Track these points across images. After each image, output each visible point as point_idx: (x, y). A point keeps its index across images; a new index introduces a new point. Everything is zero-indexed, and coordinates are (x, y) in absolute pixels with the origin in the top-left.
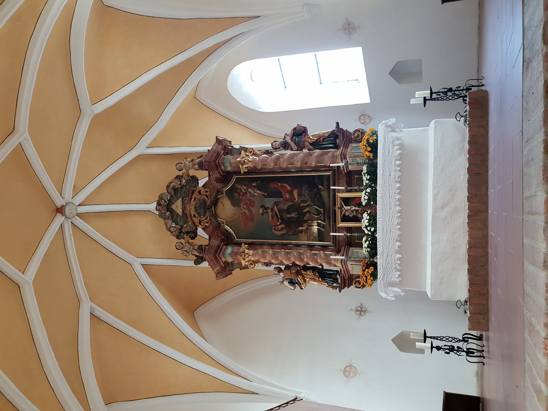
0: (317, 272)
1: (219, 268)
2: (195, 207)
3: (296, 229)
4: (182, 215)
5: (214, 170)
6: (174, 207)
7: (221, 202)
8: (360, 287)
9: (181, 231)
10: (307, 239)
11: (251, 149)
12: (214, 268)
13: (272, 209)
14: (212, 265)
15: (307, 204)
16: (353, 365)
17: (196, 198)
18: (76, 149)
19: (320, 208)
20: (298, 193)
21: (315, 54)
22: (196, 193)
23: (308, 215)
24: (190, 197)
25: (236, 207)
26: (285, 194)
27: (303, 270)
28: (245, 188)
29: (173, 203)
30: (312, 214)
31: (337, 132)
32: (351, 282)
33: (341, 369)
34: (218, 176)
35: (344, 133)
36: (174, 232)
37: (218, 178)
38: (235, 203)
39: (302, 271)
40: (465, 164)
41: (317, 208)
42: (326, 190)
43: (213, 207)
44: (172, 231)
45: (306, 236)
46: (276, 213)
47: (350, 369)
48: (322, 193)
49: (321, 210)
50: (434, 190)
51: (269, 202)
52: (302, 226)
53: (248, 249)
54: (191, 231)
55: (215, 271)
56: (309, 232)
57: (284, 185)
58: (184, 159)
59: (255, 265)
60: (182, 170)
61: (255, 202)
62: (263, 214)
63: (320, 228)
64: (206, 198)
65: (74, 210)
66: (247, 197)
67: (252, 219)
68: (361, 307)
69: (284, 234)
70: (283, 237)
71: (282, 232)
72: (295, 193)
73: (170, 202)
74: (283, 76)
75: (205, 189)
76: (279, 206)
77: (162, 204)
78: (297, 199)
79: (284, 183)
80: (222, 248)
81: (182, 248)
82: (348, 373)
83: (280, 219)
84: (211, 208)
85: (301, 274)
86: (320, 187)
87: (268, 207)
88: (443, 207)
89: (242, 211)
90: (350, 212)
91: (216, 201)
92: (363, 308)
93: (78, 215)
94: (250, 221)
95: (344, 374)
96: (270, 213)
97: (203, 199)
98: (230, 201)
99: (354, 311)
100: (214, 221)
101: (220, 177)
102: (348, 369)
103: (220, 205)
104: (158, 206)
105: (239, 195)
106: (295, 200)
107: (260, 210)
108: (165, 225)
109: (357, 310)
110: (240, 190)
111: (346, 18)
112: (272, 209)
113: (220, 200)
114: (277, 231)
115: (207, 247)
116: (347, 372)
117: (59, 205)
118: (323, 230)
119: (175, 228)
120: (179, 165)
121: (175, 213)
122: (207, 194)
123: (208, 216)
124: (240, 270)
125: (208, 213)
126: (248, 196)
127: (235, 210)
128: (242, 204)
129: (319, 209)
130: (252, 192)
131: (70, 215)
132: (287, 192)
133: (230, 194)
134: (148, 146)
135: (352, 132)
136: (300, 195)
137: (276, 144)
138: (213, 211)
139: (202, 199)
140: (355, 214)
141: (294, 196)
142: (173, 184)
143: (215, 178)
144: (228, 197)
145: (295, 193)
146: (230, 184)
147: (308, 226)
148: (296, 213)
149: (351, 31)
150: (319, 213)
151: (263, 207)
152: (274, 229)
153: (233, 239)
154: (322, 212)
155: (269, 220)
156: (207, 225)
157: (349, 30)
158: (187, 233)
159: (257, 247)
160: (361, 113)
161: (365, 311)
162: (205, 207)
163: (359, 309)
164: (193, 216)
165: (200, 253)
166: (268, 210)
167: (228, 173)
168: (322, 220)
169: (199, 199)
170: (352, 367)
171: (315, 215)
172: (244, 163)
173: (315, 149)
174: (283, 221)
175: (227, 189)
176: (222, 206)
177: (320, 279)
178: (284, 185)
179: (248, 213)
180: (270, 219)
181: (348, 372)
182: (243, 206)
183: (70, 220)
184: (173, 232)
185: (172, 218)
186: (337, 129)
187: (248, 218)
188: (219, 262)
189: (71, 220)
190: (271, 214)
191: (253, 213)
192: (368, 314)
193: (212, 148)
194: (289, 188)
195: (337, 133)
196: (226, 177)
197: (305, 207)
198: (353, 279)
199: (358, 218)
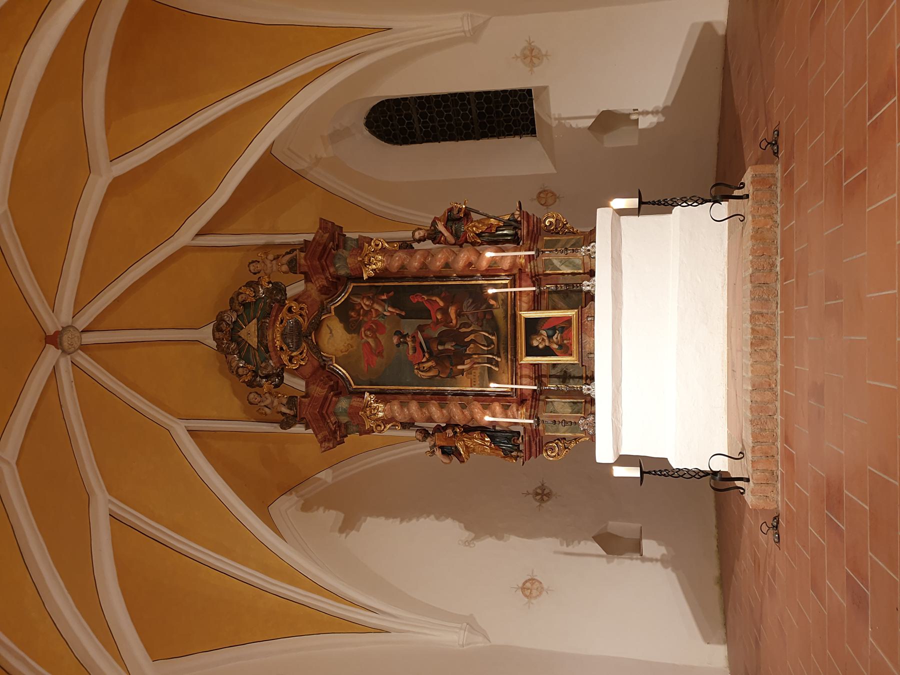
0: (487, 435)
1: (326, 433)
3: (454, 369)
6: (243, 334)
9: (255, 374)
10: (471, 383)
12: (318, 433)
13: (413, 337)
14: (315, 428)
16: (535, 578)
19: (493, 336)
20: (456, 311)
23: (472, 345)
25: (353, 335)
26: (436, 313)
27: (464, 432)
30: (478, 345)
33: (517, 585)
34: (325, 283)
37: (324, 286)
38: (351, 327)
41: (487, 335)
42: (501, 307)
44: (240, 373)
45: (469, 380)
46: (421, 343)
47: (532, 585)
48: (495, 311)
49: (493, 338)
51: (409, 326)
52: (463, 364)
54: (273, 373)
55: (320, 437)
56: (474, 373)
57: (434, 298)
60: (259, 272)
61: (386, 325)
62: (398, 345)
63: (492, 367)
64: (300, 319)
65: (76, 339)
67: (380, 354)
69: (432, 377)
71: (431, 374)
72: (452, 311)
73: (235, 327)
76: (425, 333)
77: (224, 329)
78: (454, 322)
79: (433, 295)
81: (259, 402)
82: (529, 591)
87: (408, 334)
90: (540, 341)
91: (318, 324)
92: (545, 489)
93: (84, 348)
94: (378, 356)
95: (523, 593)
98: (342, 325)
99: (531, 495)
101: (327, 285)
102: (528, 585)
103: (325, 331)
104: (217, 333)
105: (359, 315)
106: (452, 322)
107: (393, 339)
108: (228, 363)
109: (537, 494)
110: (360, 306)
111: (528, 40)
112: (414, 338)
114: (422, 372)
115: (306, 400)
117: (51, 330)
119: (245, 369)
121: (245, 344)
124: (360, 435)
125: (304, 344)
126: (374, 316)
128: (363, 329)
129: (489, 336)
130: (380, 309)
131: (70, 347)
132: (438, 309)
133: (343, 313)
136: (459, 315)
138: (314, 341)
140: (547, 344)
141: (451, 317)
143: (320, 286)
144: (338, 318)
145: (452, 311)
148: (454, 344)
150: (490, 342)
151: (398, 333)
152: (416, 369)
153: (348, 385)
154: (495, 342)
155: (409, 354)
156: (303, 363)
157: (531, 59)
159: (388, 397)
161: (549, 495)
162: (299, 334)
163: (539, 491)
166: (407, 339)
167: (338, 278)
168: (495, 354)
170: (534, 582)
171: (484, 346)
176: (329, 332)
178: (434, 298)
179: (373, 344)
180: (411, 352)
181: (529, 589)
182: (365, 331)
183: (69, 357)
184: (243, 375)
187: (374, 351)
188: (326, 423)
189: (71, 358)
190: (413, 345)
191: (382, 344)
193: (314, 239)
194: (442, 304)
195: (518, 218)
197: (468, 334)
198: (543, 445)
199: (553, 351)
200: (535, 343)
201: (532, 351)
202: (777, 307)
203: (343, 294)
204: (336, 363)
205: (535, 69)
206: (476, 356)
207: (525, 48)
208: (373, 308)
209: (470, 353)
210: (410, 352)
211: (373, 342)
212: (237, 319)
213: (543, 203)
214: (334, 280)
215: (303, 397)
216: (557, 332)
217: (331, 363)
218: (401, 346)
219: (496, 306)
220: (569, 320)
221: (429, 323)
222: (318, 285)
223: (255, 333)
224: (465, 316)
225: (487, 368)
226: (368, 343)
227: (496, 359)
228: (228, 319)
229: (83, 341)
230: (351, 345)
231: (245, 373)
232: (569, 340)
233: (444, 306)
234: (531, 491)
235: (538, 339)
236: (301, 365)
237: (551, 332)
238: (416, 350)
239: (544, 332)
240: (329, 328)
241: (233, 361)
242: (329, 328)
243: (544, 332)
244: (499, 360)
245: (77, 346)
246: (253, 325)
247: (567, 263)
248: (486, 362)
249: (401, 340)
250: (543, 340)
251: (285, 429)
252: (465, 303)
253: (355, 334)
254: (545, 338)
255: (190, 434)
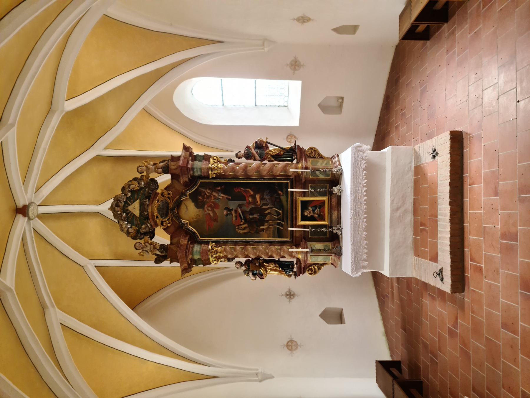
2: (158, 209)
4: (140, 216)
5: (185, 174)
7: (185, 204)
8: (313, 274)
11: (215, 157)
15: (268, 206)
16: (293, 339)
17: (160, 200)
18: (43, 145)
21: (255, 81)
22: (160, 195)
23: (269, 216)
24: (152, 199)
25: (200, 209)
26: (248, 198)
28: (209, 191)
29: (130, 205)
31: (294, 148)
32: (305, 270)
34: (187, 180)
35: (301, 150)
36: (132, 233)
37: (186, 182)
38: (199, 205)
39: (265, 263)
40: (412, 179)
41: (277, 210)
43: (176, 209)
45: (267, 234)
46: (240, 214)
47: (292, 344)
49: (280, 211)
50: (391, 197)
51: (233, 205)
52: (264, 225)
53: (216, 247)
54: (150, 232)
55: (182, 268)
56: (270, 230)
58: (145, 163)
59: (218, 261)
61: (220, 204)
62: (227, 215)
63: (280, 227)
66: (211, 199)
68: (290, 291)
70: (245, 235)
71: (245, 231)
72: (258, 197)
74: (222, 95)
75: (168, 191)
78: (259, 202)
79: (247, 188)
80: (190, 247)
82: (291, 347)
83: (244, 219)
84: (175, 210)
85: (264, 266)
86: (280, 192)
87: (232, 209)
88: (398, 209)
89: (206, 213)
90: (308, 213)
96: (234, 215)
97: (165, 201)
100: (177, 222)
102: (290, 344)
103: (183, 207)
105: (204, 198)
106: (257, 203)
108: (120, 226)
109: (287, 295)
110: (204, 193)
112: (236, 211)
113: (186, 202)
114: (240, 230)
116: (290, 346)
117: (21, 203)
118: (282, 228)
120: (140, 168)
122: (170, 196)
123: (170, 217)
125: (170, 214)
126: (213, 198)
127: (199, 212)
128: (206, 206)
129: (278, 211)
130: (216, 195)
133: (194, 198)
134: (105, 148)
135: (307, 149)
136: (262, 199)
137: (240, 154)
139: (164, 201)
140: (312, 214)
142: (133, 186)
145: (258, 197)
146: (194, 188)
147: (269, 225)
148: (258, 215)
149: (297, 67)
150: (278, 214)
151: (227, 209)
152: (237, 228)
155: (233, 220)
156: (169, 225)
158: (145, 234)
160: (289, 133)
161: (294, 295)
163: (288, 293)
164: (156, 217)
165: (161, 252)
168: (281, 220)
169: (162, 201)
172: (215, 170)
173: (275, 161)
174: (246, 221)
175: (191, 192)
176: (185, 207)
177: (281, 270)
178: (248, 190)
179: (212, 214)
180: (234, 219)
182: (207, 207)
184: (131, 232)
185: (128, 220)
186: (295, 146)
187: (212, 219)
190: (235, 215)
191: (218, 214)
192: (296, 297)
194: (252, 193)
196: (194, 180)
200: (306, 214)
201: (304, 218)
202: (360, 197)
203: (195, 186)
204: (189, 225)
205: (296, 72)
206: (271, 221)
207: (292, 61)
208: (212, 194)
209: (268, 219)
210: (233, 219)
211: (212, 213)
212: (126, 200)
213: (289, 141)
214: (191, 178)
215: (170, 245)
216: (318, 208)
217: (187, 225)
218: (228, 216)
219: (282, 194)
220: (323, 202)
221: (245, 203)
222: (183, 181)
223: (138, 208)
224: (265, 200)
225: (276, 227)
226: (209, 214)
227: (282, 223)
228: (121, 200)
229: (39, 211)
230: (199, 215)
231: (132, 231)
232: (324, 212)
233: (254, 194)
234: (284, 294)
235: (307, 212)
236: (168, 227)
237: (314, 208)
238: (237, 218)
239: (310, 208)
240: (186, 205)
241: (123, 224)
242: (186, 205)
243: (310, 208)
244: (283, 223)
245: (36, 215)
246: (137, 203)
247: (323, 173)
248: (276, 224)
249: (229, 212)
250: (310, 212)
251: (158, 263)
252: (265, 193)
253: (201, 208)
254: (311, 211)
255: (97, 269)
